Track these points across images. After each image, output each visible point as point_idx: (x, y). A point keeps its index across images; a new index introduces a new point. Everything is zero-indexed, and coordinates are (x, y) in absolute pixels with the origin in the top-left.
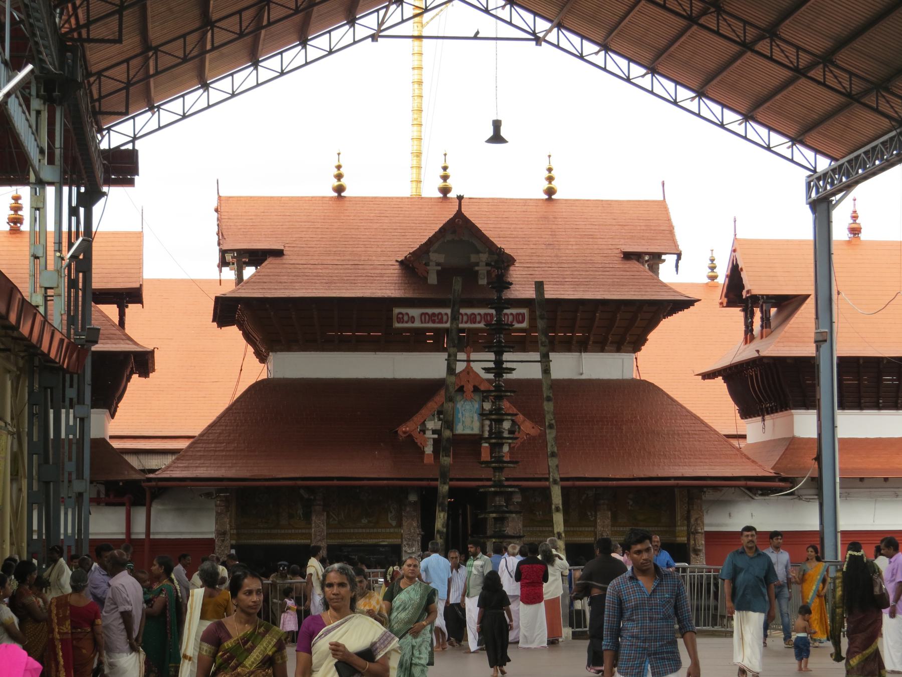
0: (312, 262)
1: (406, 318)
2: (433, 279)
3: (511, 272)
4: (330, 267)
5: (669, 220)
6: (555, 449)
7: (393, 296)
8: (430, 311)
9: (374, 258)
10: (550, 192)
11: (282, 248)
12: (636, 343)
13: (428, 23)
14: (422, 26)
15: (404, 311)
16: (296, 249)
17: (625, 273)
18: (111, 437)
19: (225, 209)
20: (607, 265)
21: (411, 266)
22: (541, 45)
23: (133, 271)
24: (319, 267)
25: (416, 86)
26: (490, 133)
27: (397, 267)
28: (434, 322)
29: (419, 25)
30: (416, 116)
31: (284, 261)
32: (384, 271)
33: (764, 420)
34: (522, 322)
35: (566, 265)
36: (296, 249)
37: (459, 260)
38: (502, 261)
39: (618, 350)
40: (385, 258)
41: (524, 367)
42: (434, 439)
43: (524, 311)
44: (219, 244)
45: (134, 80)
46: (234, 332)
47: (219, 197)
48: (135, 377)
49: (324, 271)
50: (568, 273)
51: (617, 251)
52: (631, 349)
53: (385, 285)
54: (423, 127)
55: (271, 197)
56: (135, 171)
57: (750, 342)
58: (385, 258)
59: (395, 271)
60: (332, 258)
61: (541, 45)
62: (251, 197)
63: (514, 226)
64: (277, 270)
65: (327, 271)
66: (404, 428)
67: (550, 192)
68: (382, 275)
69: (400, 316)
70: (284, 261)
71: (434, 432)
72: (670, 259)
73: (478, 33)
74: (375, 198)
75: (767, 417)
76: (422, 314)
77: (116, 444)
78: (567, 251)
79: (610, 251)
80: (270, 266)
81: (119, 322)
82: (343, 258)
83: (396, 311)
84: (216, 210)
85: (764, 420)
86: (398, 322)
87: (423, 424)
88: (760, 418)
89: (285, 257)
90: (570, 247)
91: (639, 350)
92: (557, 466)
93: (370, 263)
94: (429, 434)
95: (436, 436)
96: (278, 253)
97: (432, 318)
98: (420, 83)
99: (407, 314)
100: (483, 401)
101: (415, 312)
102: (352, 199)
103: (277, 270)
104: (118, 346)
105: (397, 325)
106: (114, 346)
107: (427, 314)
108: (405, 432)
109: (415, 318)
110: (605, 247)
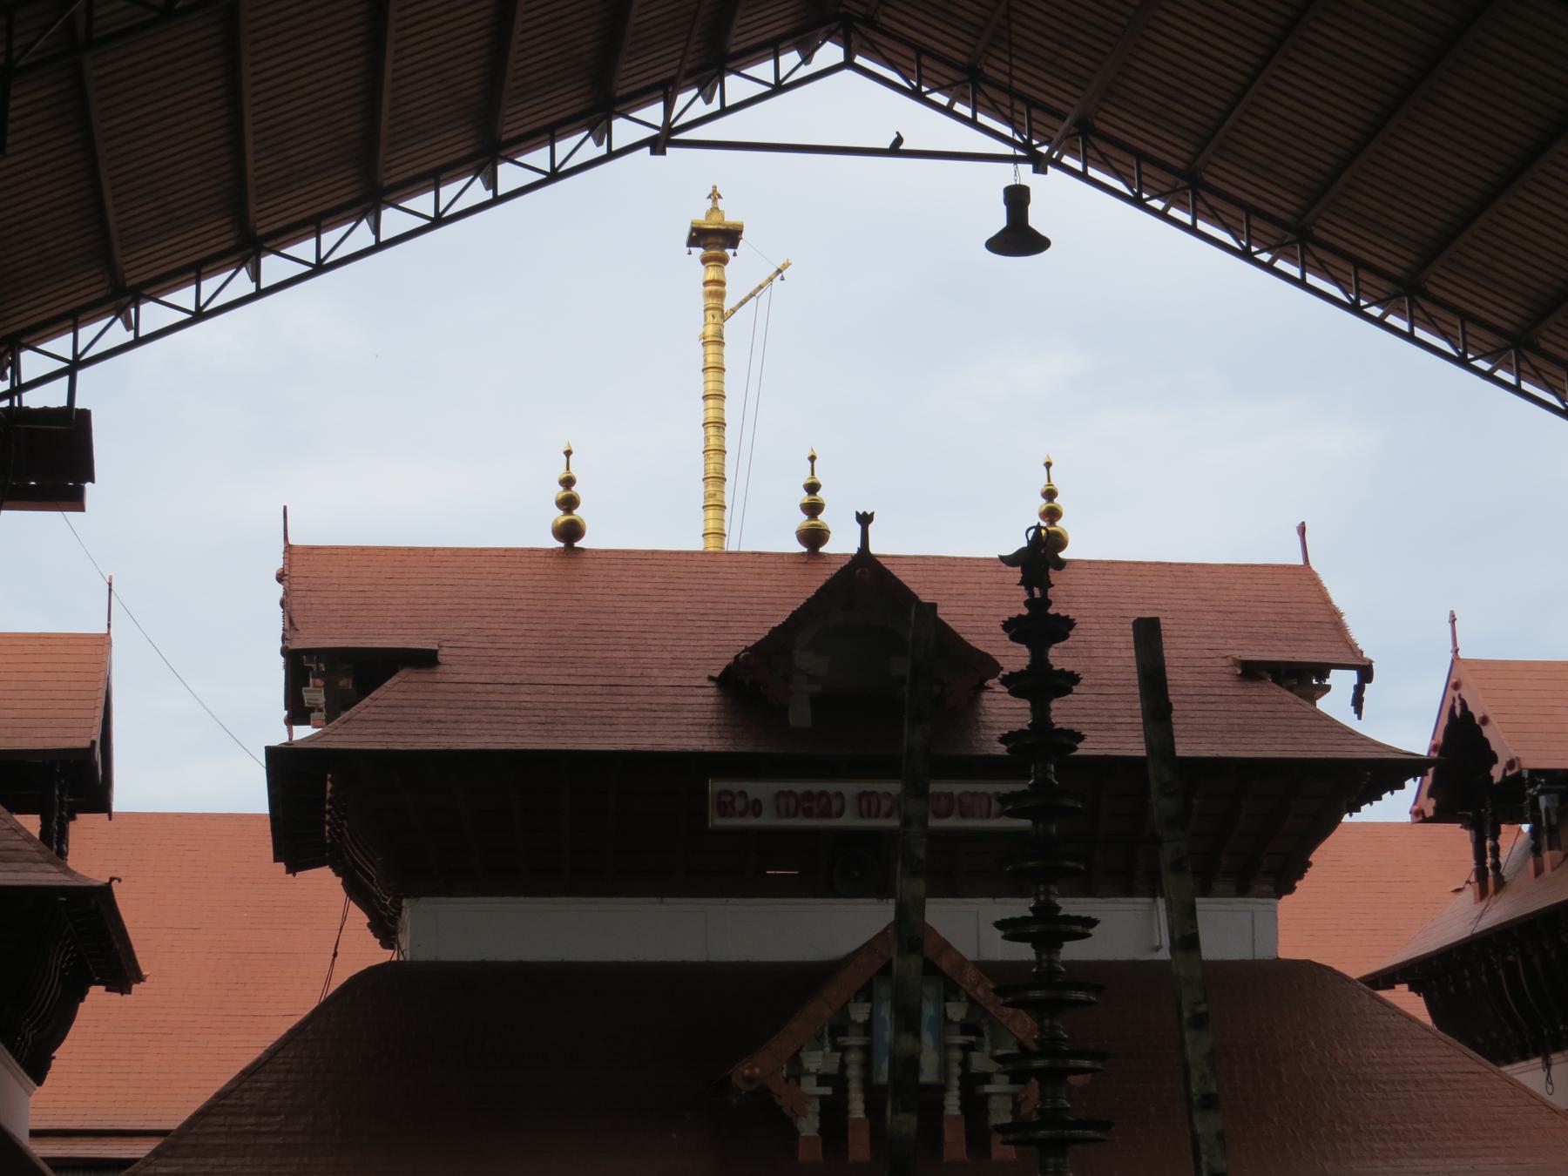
0: (506, 679)
1: (740, 804)
2: (800, 715)
3: (985, 704)
4: (551, 689)
5: (1326, 601)
6: (1213, 1088)
7: (707, 749)
8: (800, 787)
10: (570, 532)
11: (430, 645)
12: (1281, 870)
13: (733, 311)
15: (735, 786)
16: (467, 652)
17: (1251, 707)
18: (35, 1134)
19: (304, 573)
20: (1209, 691)
21: (747, 683)
22: (1045, 172)
23: (76, 714)
24: (524, 689)
25: (712, 431)
26: (998, 220)
27: (713, 691)
28: (809, 814)
29: (717, 314)
30: (711, 489)
31: (438, 677)
32: (680, 700)
33: (1548, 1066)
35: (1112, 690)
37: (862, 672)
38: (1274, 681)
39: (1242, 891)
40: (681, 673)
41: (1123, 930)
42: (823, 1098)
44: (284, 639)
45: (22, 63)
46: (324, 883)
47: (289, 548)
48: (96, 993)
49: (535, 698)
50: (1122, 706)
51: (1224, 662)
52: (1270, 888)
53: (687, 724)
54: (727, 512)
55: (411, 549)
56: (84, 470)
57: (1496, 892)
58: (681, 673)
59: (707, 698)
60: (555, 671)
61: (1045, 172)
62: (363, 549)
63: (977, 611)
64: (421, 696)
66: (749, 1070)
67: (570, 532)
68: (676, 708)
69: (727, 799)
70: (438, 677)
71: (822, 1080)
72: (1342, 681)
73: (899, 140)
74: (654, 552)
75: (1555, 1057)
76: (780, 794)
77: (42, 1150)
78: (1110, 662)
79: (1208, 662)
80: (404, 687)
81: (41, 833)
82: (580, 671)
83: (715, 786)
84: (280, 578)
85: (1548, 1066)
86: (723, 815)
87: (796, 1060)
88: (1538, 1061)
89: (440, 668)
90: (1115, 653)
91: (1290, 889)
92: (1220, 1136)
93: (647, 682)
94: (809, 1086)
95: (827, 1091)
96: (425, 660)
97: (805, 804)
98: (720, 425)
99: (743, 794)
100: (947, 1000)
102: (597, 554)
103: (421, 696)
104: (21, 876)
105: (717, 821)
106: (12, 876)
107: (791, 793)
108: (749, 1080)
109: (765, 804)
110: (1196, 654)
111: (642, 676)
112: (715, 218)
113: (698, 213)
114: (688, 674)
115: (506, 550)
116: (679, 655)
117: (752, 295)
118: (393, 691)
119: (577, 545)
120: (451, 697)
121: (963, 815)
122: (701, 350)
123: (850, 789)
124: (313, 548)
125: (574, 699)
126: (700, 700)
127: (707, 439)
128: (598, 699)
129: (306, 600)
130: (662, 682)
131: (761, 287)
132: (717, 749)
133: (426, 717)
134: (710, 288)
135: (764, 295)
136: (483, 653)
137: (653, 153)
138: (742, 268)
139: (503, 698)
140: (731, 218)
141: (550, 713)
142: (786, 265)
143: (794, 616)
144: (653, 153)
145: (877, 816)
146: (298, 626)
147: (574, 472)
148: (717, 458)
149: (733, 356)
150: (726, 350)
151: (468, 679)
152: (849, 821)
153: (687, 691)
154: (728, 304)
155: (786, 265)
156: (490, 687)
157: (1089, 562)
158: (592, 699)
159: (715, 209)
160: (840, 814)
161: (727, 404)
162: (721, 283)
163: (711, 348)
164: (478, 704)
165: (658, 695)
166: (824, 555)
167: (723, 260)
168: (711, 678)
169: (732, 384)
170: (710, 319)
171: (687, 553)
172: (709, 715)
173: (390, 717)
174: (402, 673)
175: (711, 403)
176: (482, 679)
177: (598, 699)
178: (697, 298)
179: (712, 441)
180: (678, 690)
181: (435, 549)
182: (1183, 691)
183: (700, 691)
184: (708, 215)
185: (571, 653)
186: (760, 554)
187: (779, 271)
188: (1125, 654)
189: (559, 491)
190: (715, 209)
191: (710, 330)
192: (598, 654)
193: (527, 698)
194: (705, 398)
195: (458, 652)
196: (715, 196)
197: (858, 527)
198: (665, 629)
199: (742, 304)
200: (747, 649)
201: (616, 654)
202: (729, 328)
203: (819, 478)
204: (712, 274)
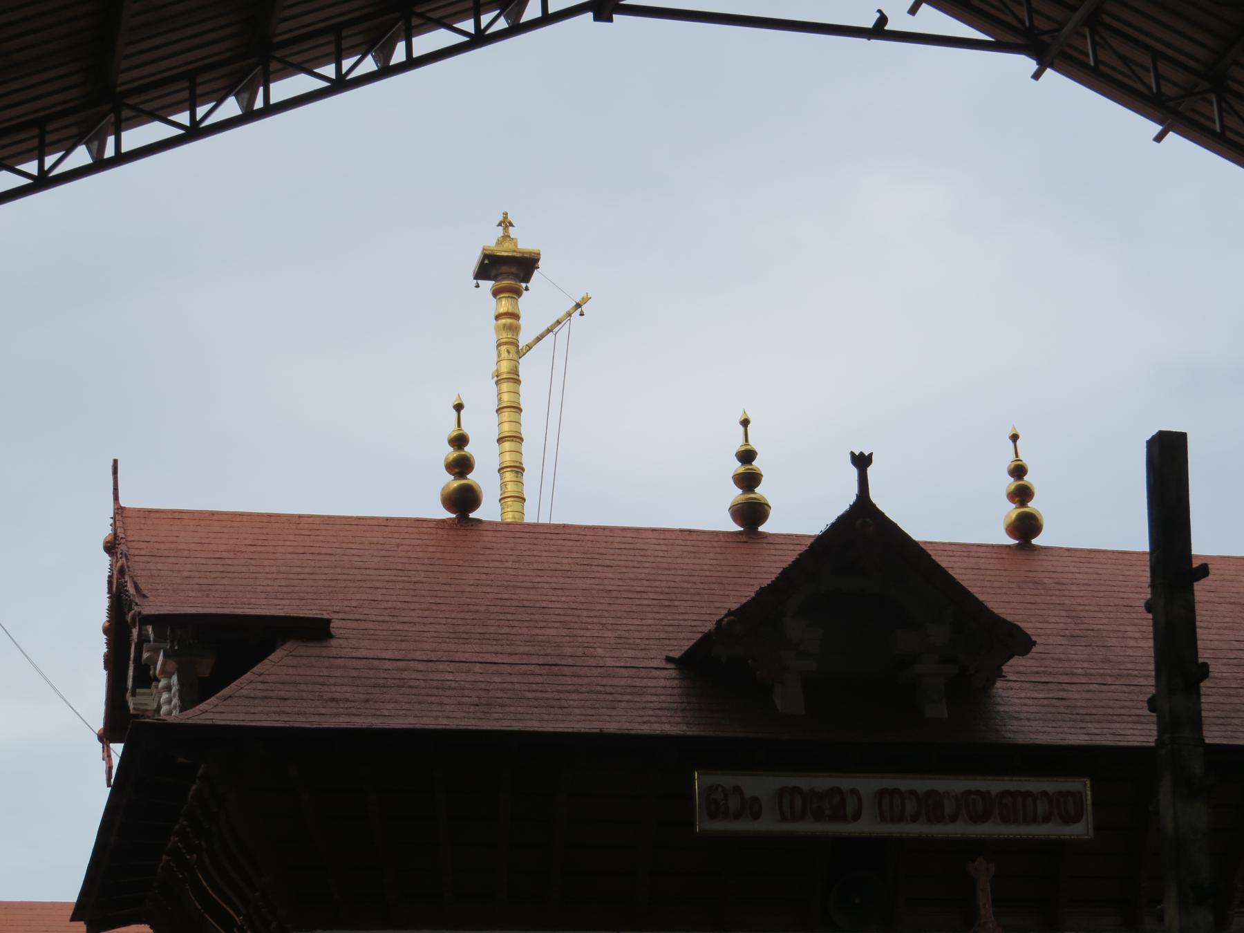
2: (789, 699)
4: (477, 668)
8: (806, 782)
9: (600, 651)
13: (529, 347)
14: (518, 352)
15: (728, 780)
16: (363, 625)
21: (711, 664)
25: (509, 476)
27: (673, 673)
28: (818, 817)
32: (638, 682)
34: (1076, 819)
36: (363, 625)
40: (631, 653)
43: (1083, 786)
47: (119, 511)
49: (460, 677)
53: (650, 707)
55: (270, 515)
58: (631, 653)
59: (665, 682)
60: (477, 648)
62: (212, 513)
65: (471, 678)
70: (334, 652)
73: (883, 19)
74: (565, 526)
76: (782, 791)
78: (1129, 652)
82: (509, 649)
84: (110, 547)
86: (713, 816)
89: (334, 642)
93: (592, 662)
96: (314, 631)
97: (932, 807)
98: (518, 469)
99: (737, 789)
101: (761, 786)
105: (703, 825)
107: (797, 790)
111: (584, 655)
112: (508, 245)
113: (490, 239)
114: (639, 654)
115: (388, 519)
116: (623, 634)
117: (549, 331)
118: (279, 664)
119: (472, 515)
120: (354, 673)
121: (1005, 820)
122: (494, 388)
123: (868, 785)
124: (150, 511)
125: (508, 679)
126: (663, 683)
127: (503, 485)
128: (538, 679)
129: (152, 566)
130: (609, 662)
131: (558, 322)
132: (695, 733)
133: (327, 696)
134: (503, 321)
135: (563, 331)
136: (384, 626)
137: (596, 19)
138: (538, 301)
139: (419, 676)
140: (524, 243)
141: (483, 694)
142: (586, 299)
143: (786, 573)
144: (596, 19)
145: (901, 819)
146: (145, 592)
147: (466, 429)
148: (516, 506)
149: (529, 394)
150: (523, 388)
151: (371, 654)
152: (867, 826)
153: (644, 673)
154: (523, 341)
155: (586, 299)
156: (401, 664)
157: (1068, 550)
158: (531, 679)
159: (506, 237)
160: (857, 816)
161: (525, 447)
162: (515, 316)
163: (505, 386)
164: (391, 682)
165: (609, 676)
166: (764, 535)
167: (517, 293)
168: (669, 659)
169: (530, 426)
170: (504, 355)
171: (604, 528)
172: (677, 699)
173: (282, 694)
174: (289, 646)
175: (507, 445)
176: (388, 654)
177: (538, 679)
178: (489, 333)
179: (511, 488)
180: (632, 672)
181: (300, 516)
182: (1224, 683)
183: (658, 673)
184: (499, 243)
185: (492, 629)
186: (690, 531)
187: (578, 306)
188: (1142, 644)
189: (450, 452)
190: (506, 237)
191: (505, 367)
192: (525, 631)
193: (450, 677)
194: (501, 440)
195: (354, 625)
196: (506, 223)
197: (854, 472)
198: (598, 607)
199: (539, 339)
200: (730, 613)
201: (548, 632)
202: (526, 366)
203: (754, 444)
204: (505, 305)
